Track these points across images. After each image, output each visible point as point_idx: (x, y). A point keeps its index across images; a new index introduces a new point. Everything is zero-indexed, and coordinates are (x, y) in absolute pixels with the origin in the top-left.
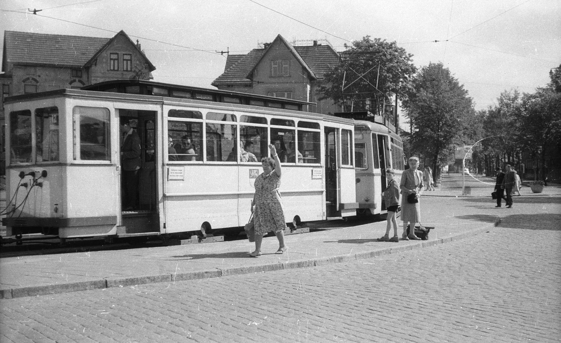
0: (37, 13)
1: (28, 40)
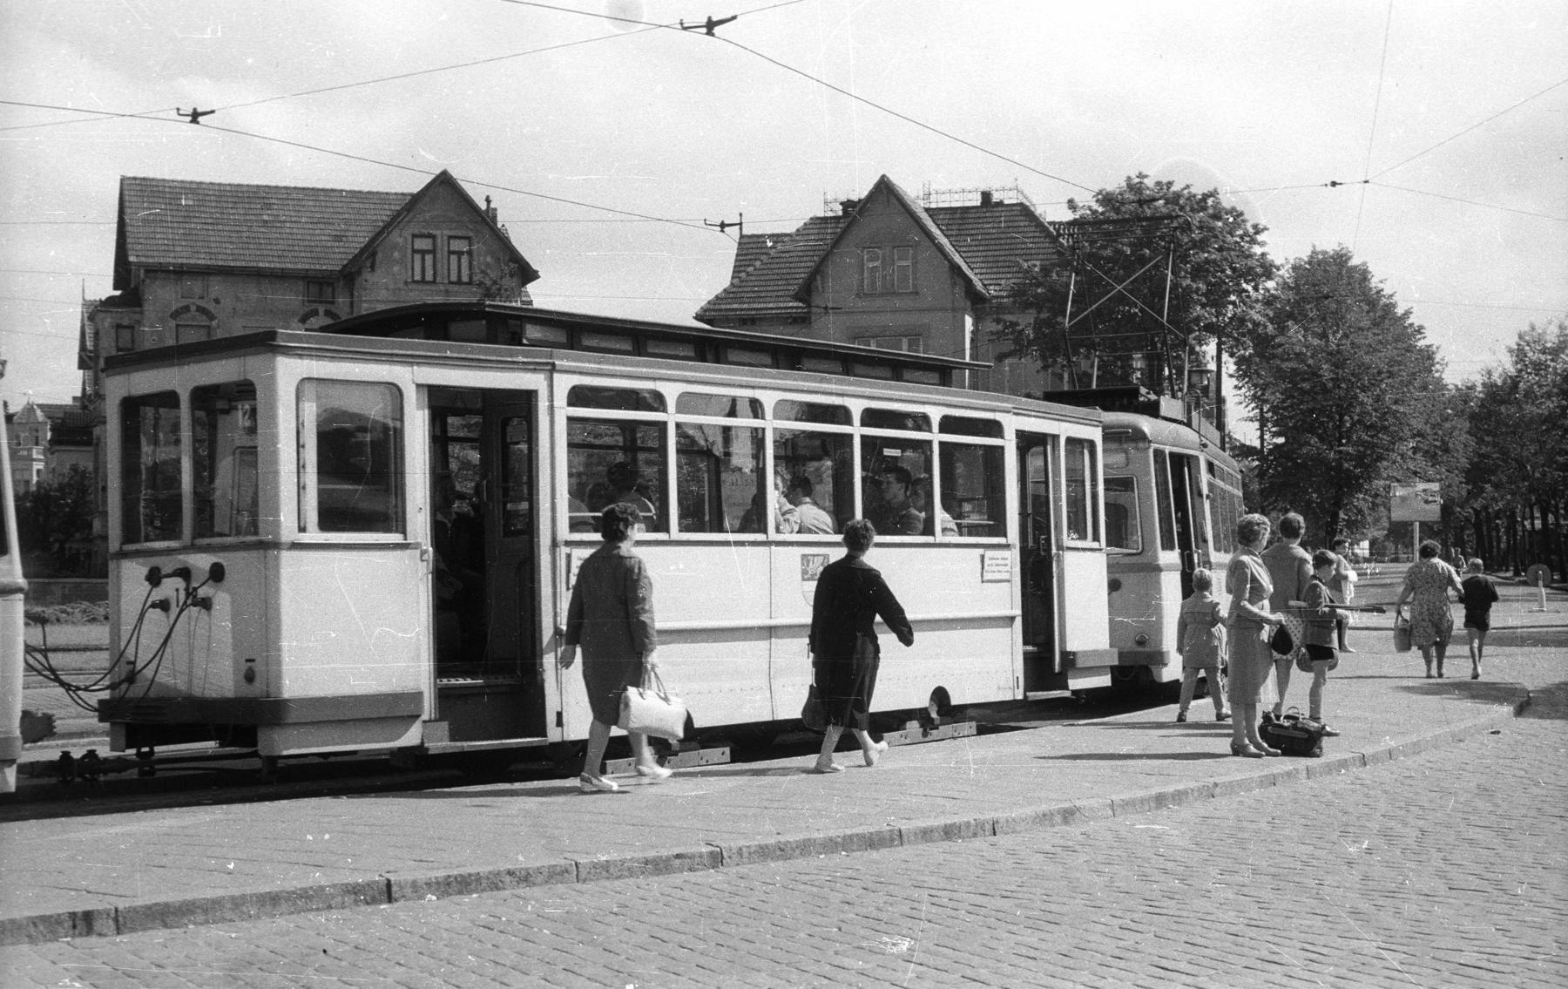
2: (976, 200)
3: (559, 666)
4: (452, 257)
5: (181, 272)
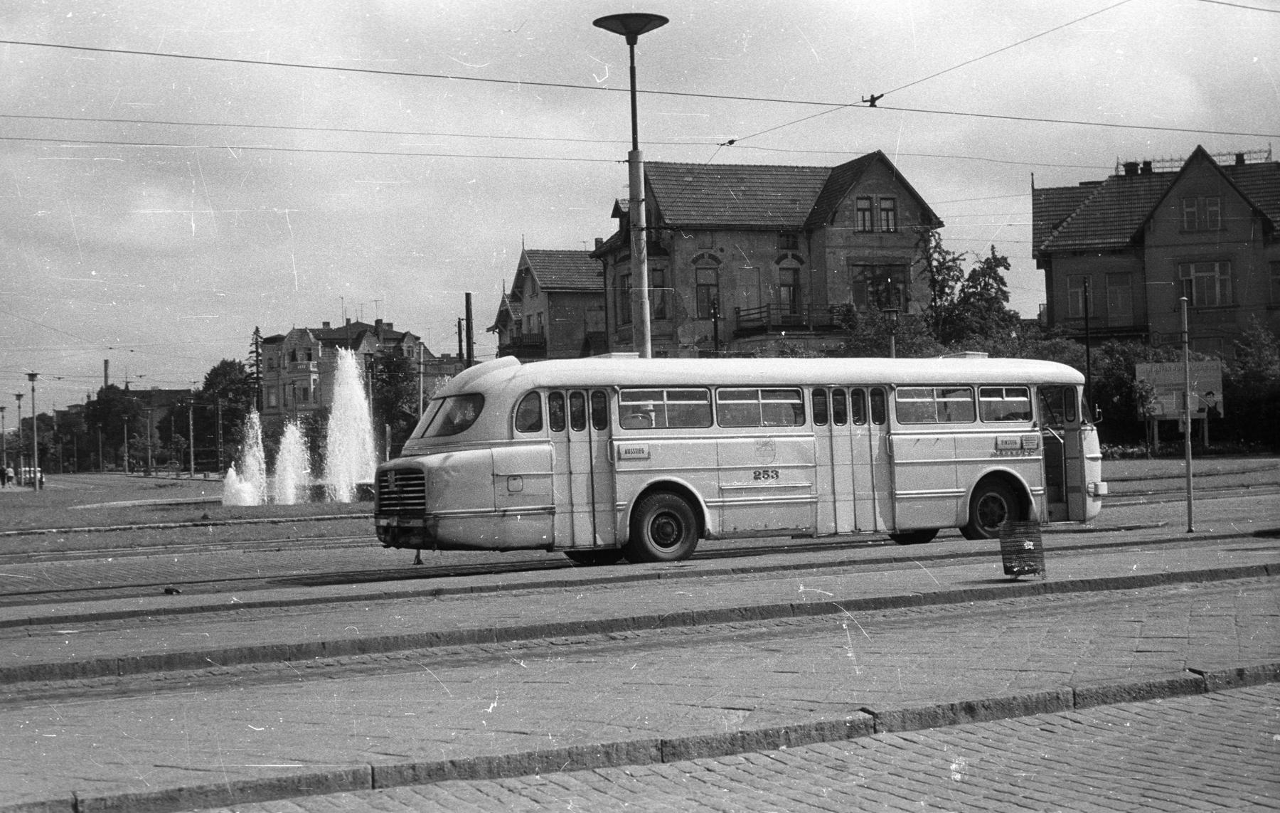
0: (877, 103)
1: (686, 179)
2: (1232, 161)
3: (1035, 579)
4: (883, 213)
5: (697, 230)
